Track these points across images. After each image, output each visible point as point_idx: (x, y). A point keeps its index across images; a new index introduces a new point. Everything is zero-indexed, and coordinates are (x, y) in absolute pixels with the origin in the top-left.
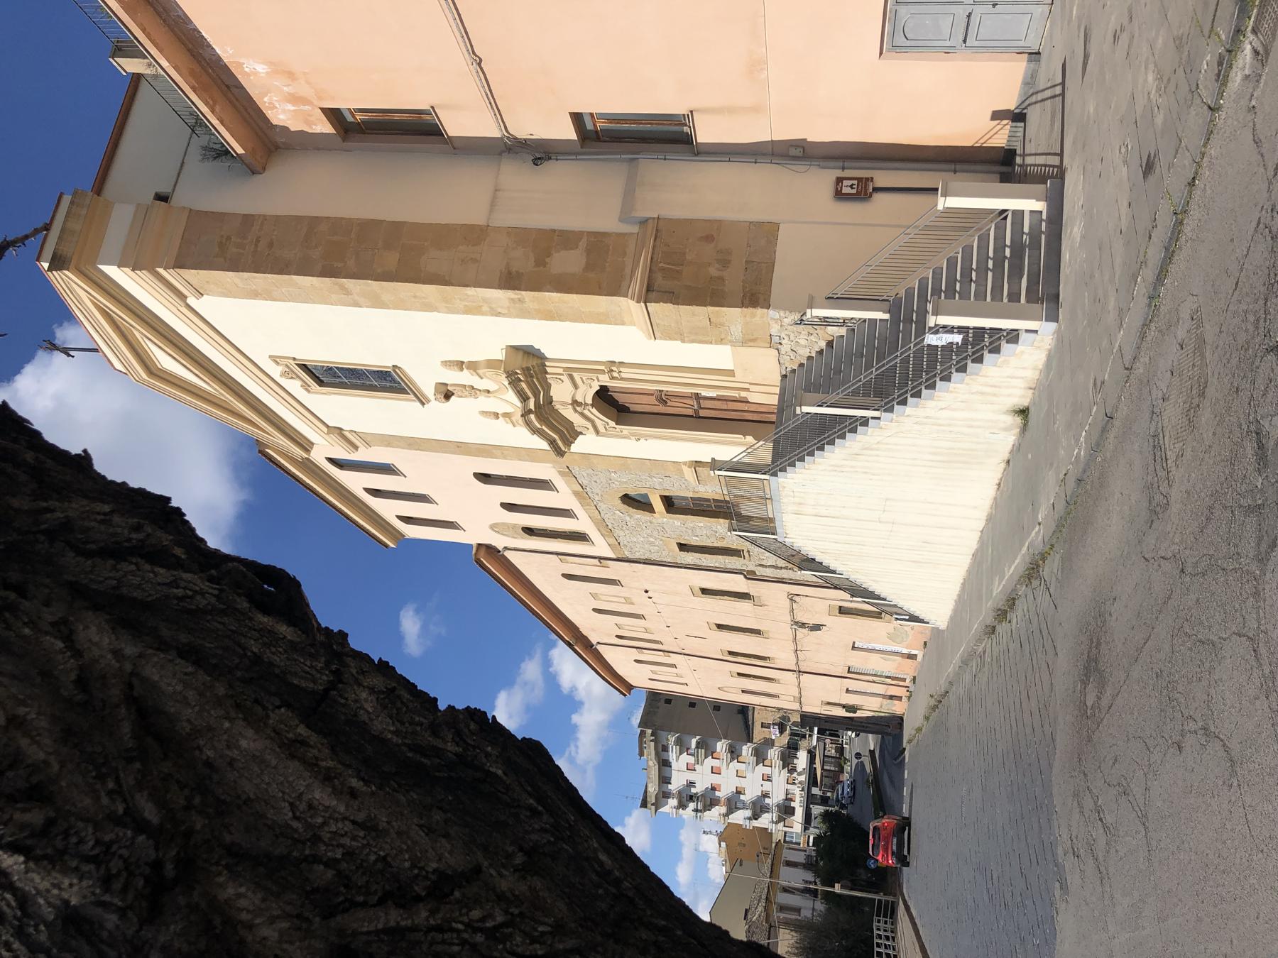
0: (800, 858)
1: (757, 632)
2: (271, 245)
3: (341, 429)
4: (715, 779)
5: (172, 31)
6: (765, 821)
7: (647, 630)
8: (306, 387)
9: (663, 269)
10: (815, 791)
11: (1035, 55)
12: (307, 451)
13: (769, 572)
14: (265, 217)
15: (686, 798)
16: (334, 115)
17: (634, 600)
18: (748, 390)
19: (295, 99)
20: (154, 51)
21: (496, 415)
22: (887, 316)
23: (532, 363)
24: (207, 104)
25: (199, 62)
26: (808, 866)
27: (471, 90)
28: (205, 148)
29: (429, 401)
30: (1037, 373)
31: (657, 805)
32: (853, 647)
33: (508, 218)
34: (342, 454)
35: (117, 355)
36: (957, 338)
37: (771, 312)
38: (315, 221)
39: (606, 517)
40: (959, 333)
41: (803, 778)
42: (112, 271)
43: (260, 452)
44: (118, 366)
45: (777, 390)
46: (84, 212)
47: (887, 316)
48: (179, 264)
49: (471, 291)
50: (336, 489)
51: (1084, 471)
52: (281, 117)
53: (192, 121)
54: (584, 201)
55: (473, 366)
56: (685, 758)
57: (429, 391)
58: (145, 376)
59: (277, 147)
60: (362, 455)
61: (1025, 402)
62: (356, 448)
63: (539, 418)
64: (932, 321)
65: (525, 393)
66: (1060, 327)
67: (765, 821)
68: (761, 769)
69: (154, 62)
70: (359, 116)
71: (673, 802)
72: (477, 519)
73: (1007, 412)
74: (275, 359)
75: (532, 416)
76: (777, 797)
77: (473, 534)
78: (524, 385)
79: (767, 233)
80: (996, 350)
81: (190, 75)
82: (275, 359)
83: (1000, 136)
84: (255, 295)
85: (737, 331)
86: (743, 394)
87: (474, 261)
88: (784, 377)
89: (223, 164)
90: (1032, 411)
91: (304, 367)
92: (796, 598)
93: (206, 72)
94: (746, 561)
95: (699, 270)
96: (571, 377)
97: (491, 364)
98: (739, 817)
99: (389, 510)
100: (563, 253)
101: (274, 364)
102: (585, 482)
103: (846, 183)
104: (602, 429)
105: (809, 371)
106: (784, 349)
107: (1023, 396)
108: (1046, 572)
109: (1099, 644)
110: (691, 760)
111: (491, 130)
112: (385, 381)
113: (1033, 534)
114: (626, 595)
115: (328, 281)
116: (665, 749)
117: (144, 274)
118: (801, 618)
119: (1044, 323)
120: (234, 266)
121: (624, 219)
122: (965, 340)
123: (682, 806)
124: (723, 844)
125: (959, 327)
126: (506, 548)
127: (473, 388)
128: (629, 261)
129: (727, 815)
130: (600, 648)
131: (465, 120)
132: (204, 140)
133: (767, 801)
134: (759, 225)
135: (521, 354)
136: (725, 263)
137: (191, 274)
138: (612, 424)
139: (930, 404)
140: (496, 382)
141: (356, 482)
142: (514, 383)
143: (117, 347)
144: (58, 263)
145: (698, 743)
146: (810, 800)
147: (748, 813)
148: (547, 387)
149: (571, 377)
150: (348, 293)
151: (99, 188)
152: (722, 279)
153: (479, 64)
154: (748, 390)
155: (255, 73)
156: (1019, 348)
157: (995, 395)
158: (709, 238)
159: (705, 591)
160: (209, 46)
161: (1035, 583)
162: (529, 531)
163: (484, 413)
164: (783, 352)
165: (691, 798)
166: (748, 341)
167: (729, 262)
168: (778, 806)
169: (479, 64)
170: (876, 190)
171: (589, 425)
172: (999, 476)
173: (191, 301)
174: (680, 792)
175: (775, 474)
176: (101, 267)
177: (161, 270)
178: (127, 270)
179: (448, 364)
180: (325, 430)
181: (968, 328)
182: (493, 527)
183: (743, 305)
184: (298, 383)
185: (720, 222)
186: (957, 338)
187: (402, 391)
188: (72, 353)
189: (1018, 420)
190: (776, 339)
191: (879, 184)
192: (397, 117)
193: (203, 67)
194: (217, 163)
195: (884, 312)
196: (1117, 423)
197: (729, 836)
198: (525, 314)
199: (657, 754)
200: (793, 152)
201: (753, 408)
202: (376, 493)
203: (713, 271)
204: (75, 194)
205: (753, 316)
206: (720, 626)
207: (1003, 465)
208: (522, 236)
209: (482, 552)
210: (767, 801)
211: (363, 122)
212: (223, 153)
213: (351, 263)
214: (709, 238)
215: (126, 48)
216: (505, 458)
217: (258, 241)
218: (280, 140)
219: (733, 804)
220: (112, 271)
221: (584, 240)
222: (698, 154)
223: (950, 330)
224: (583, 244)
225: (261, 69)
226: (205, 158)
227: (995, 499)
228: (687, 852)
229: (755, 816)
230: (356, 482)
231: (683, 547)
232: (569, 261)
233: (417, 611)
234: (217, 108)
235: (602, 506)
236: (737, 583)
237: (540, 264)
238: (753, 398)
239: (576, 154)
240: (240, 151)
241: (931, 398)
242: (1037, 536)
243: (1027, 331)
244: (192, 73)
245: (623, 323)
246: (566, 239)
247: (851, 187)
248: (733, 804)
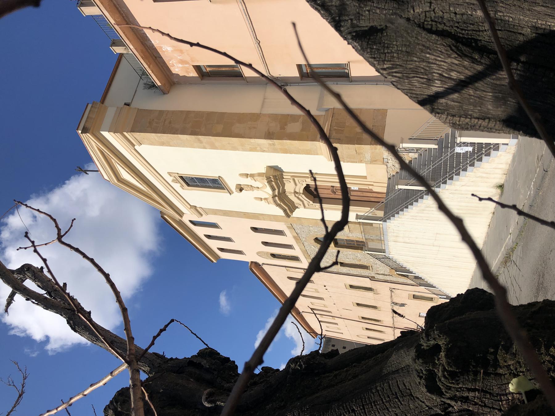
1: (375, 307)
2: (170, 123)
3: (196, 207)
5: (135, 34)
7: (325, 306)
8: (182, 186)
12: (181, 217)
13: (381, 277)
16: (198, 68)
17: (319, 290)
18: (373, 185)
19: (182, 62)
20: (128, 42)
21: (261, 199)
22: (436, 147)
24: (147, 64)
25: (145, 47)
28: (145, 84)
29: (233, 193)
30: (508, 166)
32: (420, 316)
33: (270, 110)
34: (196, 218)
35: (106, 173)
36: (470, 149)
38: (188, 112)
39: (307, 249)
40: (471, 146)
42: (106, 134)
43: (162, 217)
44: (106, 177)
45: (386, 185)
46: (96, 110)
47: (436, 147)
48: (133, 131)
49: (253, 141)
50: (193, 236)
51: (533, 200)
52: (177, 70)
53: (140, 73)
55: (252, 176)
57: (232, 186)
58: (116, 182)
60: (205, 219)
61: (501, 181)
62: (202, 215)
63: (279, 199)
64: (459, 140)
65: (274, 187)
66: (519, 141)
69: (129, 48)
70: (208, 69)
72: (251, 249)
73: (493, 187)
74: (169, 174)
75: (277, 198)
77: (248, 258)
78: (273, 183)
79: (382, 113)
80: (488, 155)
81: (142, 52)
82: (169, 174)
84: (163, 144)
85: (368, 156)
86: (371, 187)
87: (254, 128)
88: (389, 178)
89: (153, 90)
90: (506, 188)
91: (182, 177)
92: (393, 290)
94: (370, 272)
96: (294, 180)
97: (260, 175)
99: (214, 245)
101: (169, 176)
102: (298, 231)
104: (306, 205)
106: (389, 165)
107: (501, 178)
108: (514, 258)
109: (544, 275)
112: (215, 184)
113: (508, 239)
114: (316, 288)
115: (193, 137)
117: (118, 135)
118: (394, 301)
119: (511, 139)
120: (155, 131)
122: (474, 150)
125: (471, 143)
126: (263, 264)
127: (251, 186)
130: (303, 314)
132: (145, 81)
135: (273, 169)
137: (137, 135)
138: (311, 202)
139: (457, 183)
140: (262, 183)
141: (201, 232)
142: (269, 182)
143: (106, 168)
144: (85, 131)
148: (283, 185)
149: (294, 180)
150: (201, 142)
151: (103, 101)
153: (259, 44)
154: (373, 185)
155: (167, 51)
156: (499, 153)
157: (487, 178)
159: (351, 287)
160: (149, 40)
161: (508, 264)
162: (273, 256)
163: (256, 198)
164: (389, 166)
166: (373, 161)
169: (259, 44)
171: (301, 203)
172: (489, 221)
173: (137, 147)
175: (385, 221)
176: (102, 132)
177: (125, 133)
178: (112, 133)
179: (241, 175)
180: (189, 207)
181: (475, 143)
182: (258, 253)
184: (179, 185)
186: (470, 149)
187: (222, 188)
188: (88, 172)
189: (499, 191)
190: (386, 160)
192: (224, 69)
193: (146, 49)
194: (150, 90)
195: (436, 145)
196: (549, 173)
198: (275, 151)
201: (375, 195)
202: (209, 237)
204: (93, 103)
205: (376, 149)
206: (358, 304)
207: (491, 215)
208: (275, 117)
209: (253, 264)
211: (210, 72)
212: (153, 86)
215: (117, 42)
216: (264, 220)
217: (165, 121)
218: (175, 80)
220: (106, 134)
221: (302, 118)
222: (352, 81)
223: (465, 144)
226: (145, 88)
227: (487, 233)
230: (201, 232)
233: (226, 295)
234: (151, 66)
235: (306, 244)
236: (366, 283)
238: (375, 189)
239: (298, 83)
240: (159, 84)
241: (458, 180)
242: (509, 240)
243: (503, 144)
244: (142, 51)
245: (317, 154)
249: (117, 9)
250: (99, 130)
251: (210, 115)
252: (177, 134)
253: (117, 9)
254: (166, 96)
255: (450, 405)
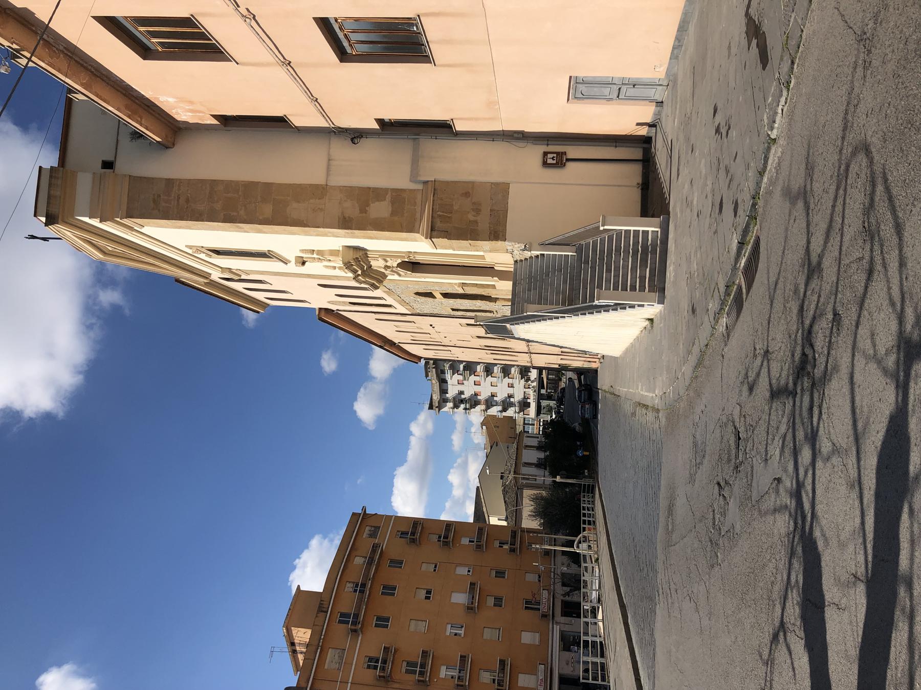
0: (534, 442)
2: (187, 201)
4: (477, 389)
6: (510, 412)
9: (440, 216)
10: (543, 391)
11: (660, 104)
14: (181, 181)
15: (458, 401)
23: (359, 254)
26: (539, 448)
27: (311, 108)
31: (440, 407)
33: (338, 180)
37: (506, 243)
38: (214, 183)
41: (535, 384)
46: (59, 182)
48: (130, 216)
54: (384, 168)
56: (457, 377)
59: (180, 129)
67: (510, 412)
68: (507, 381)
71: (450, 405)
76: (518, 397)
79: (501, 190)
83: (643, 131)
85: (488, 248)
87: (321, 210)
88: (516, 262)
93: (134, 102)
95: (464, 213)
98: (494, 411)
100: (377, 203)
103: (550, 156)
105: (531, 266)
110: (461, 378)
111: (322, 123)
116: (443, 372)
121: (414, 178)
123: (456, 406)
124: (484, 427)
128: (418, 209)
129: (486, 410)
131: (304, 116)
133: (512, 400)
134: (497, 184)
136: (478, 211)
145: (464, 367)
146: (540, 397)
147: (500, 408)
152: (476, 222)
158: (467, 194)
165: (462, 401)
167: (480, 210)
168: (519, 402)
170: (568, 160)
174: (454, 398)
183: (490, 239)
185: (473, 183)
191: (570, 156)
197: (488, 422)
199: (438, 376)
200: (516, 135)
203: (471, 217)
208: (351, 192)
210: (512, 400)
213: (242, 212)
214: (467, 194)
219: (489, 403)
224: (388, 197)
225: (171, 100)
228: (459, 426)
229: (505, 410)
231: (453, 310)
232: (380, 209)
237: (360, 210)
240: (158, 139)
244: (127, 107)
246: (377, 194)
247: (553, 158)
248: (489, 403)
249: (82, 65)
250: (73, 216)
251: (250, 187)
252: (203, 221)
253: (82, 65)
254: (170, 151)
255: (579, 646)
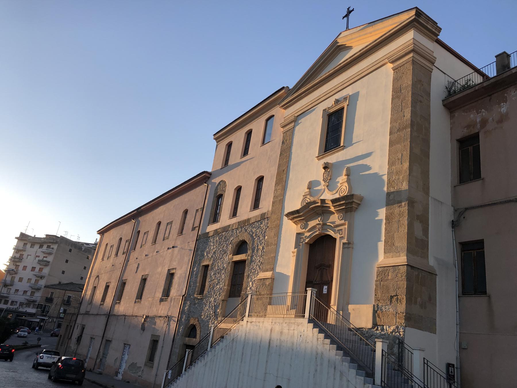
182: (223, 183)
203: (419, 299)
214: (430, 299)
217: (422, 97)
221: (426, 240)
246: (426, 231)
247: (451, 372)
